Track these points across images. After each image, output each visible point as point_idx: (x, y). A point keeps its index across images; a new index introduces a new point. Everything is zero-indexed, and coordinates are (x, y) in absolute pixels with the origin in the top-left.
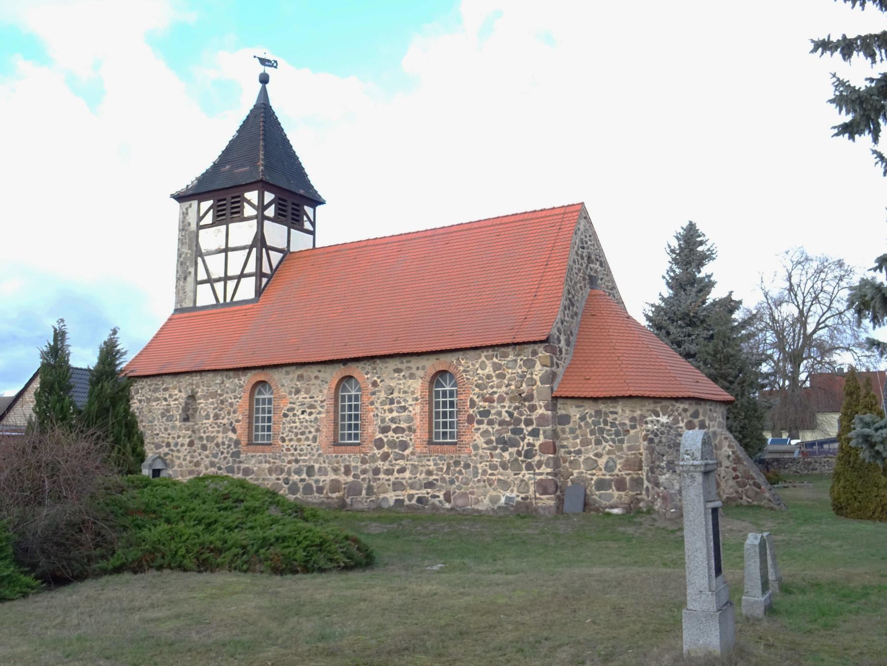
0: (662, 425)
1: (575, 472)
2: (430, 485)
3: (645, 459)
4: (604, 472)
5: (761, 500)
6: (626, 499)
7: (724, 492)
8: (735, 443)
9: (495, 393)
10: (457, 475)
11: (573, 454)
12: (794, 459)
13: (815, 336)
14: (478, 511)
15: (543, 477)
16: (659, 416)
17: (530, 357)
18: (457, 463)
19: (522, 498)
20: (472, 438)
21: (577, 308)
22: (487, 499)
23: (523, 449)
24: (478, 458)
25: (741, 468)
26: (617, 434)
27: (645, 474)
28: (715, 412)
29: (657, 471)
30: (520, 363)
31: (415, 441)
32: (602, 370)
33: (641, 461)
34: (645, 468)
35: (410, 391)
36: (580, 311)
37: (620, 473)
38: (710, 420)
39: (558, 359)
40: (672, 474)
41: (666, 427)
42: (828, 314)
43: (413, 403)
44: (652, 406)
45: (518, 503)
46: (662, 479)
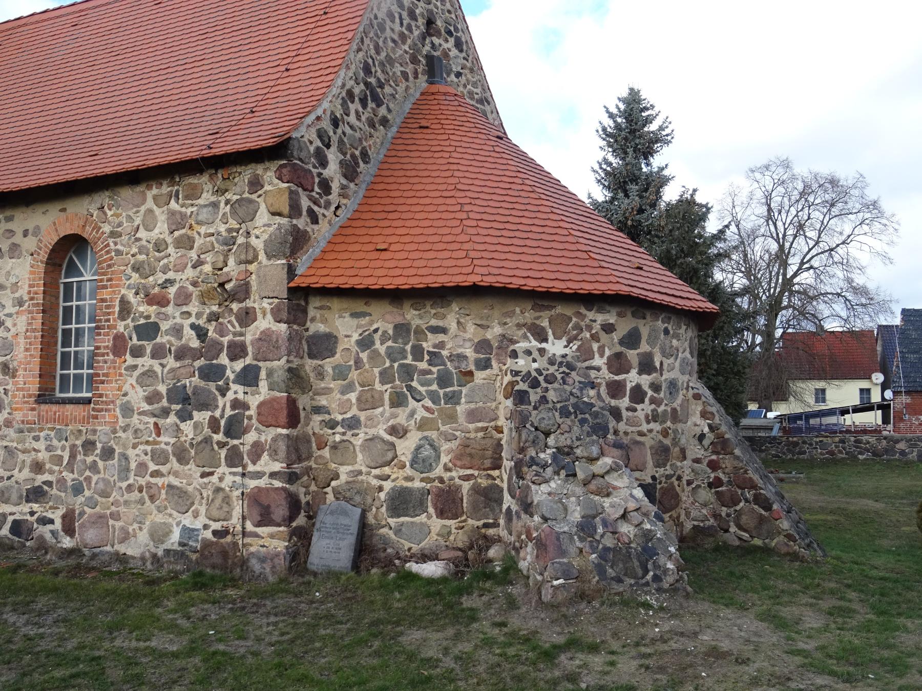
0: (552, 362)
1: (344, 470)
2: (36, 494)
3: (509, 443)
4: (408, 471)
5: (771, 535)
6: (460, 538)
7: (688, 514)
8: (715, 408)
9: (170, 282)
10: (88, 473)
11: (339, 429)
12: (775, 438)
13: (796, 280)
14: (122, 559)
15: (262, 483)
16: (545, 340)
17: (246, 195)
18: (89, 445)
19: (215, 533)
20: (120, 389)
21: (389, 110)
22: (145, 531)
23: (222, 416)
24: (130, 433)
25: (728, 463)
26: (444, 380)
27: (505, 477)
28: (677, 336)
29: (529, 473)
30: (225, 209)
31: (14, 396)
32: (453, 263)
33: (499, 446)
34: (508, 464)
35: (8, 284)
36: (396, 119)
37: (446, 475)
38: (664, 354)
39: (316, 203)
40: (566, 481)
41: (561, 364)
42: (814, 252)
43: (13, 310)
44: (529, 316)
45: (206, 544)
46: (540, 494)
